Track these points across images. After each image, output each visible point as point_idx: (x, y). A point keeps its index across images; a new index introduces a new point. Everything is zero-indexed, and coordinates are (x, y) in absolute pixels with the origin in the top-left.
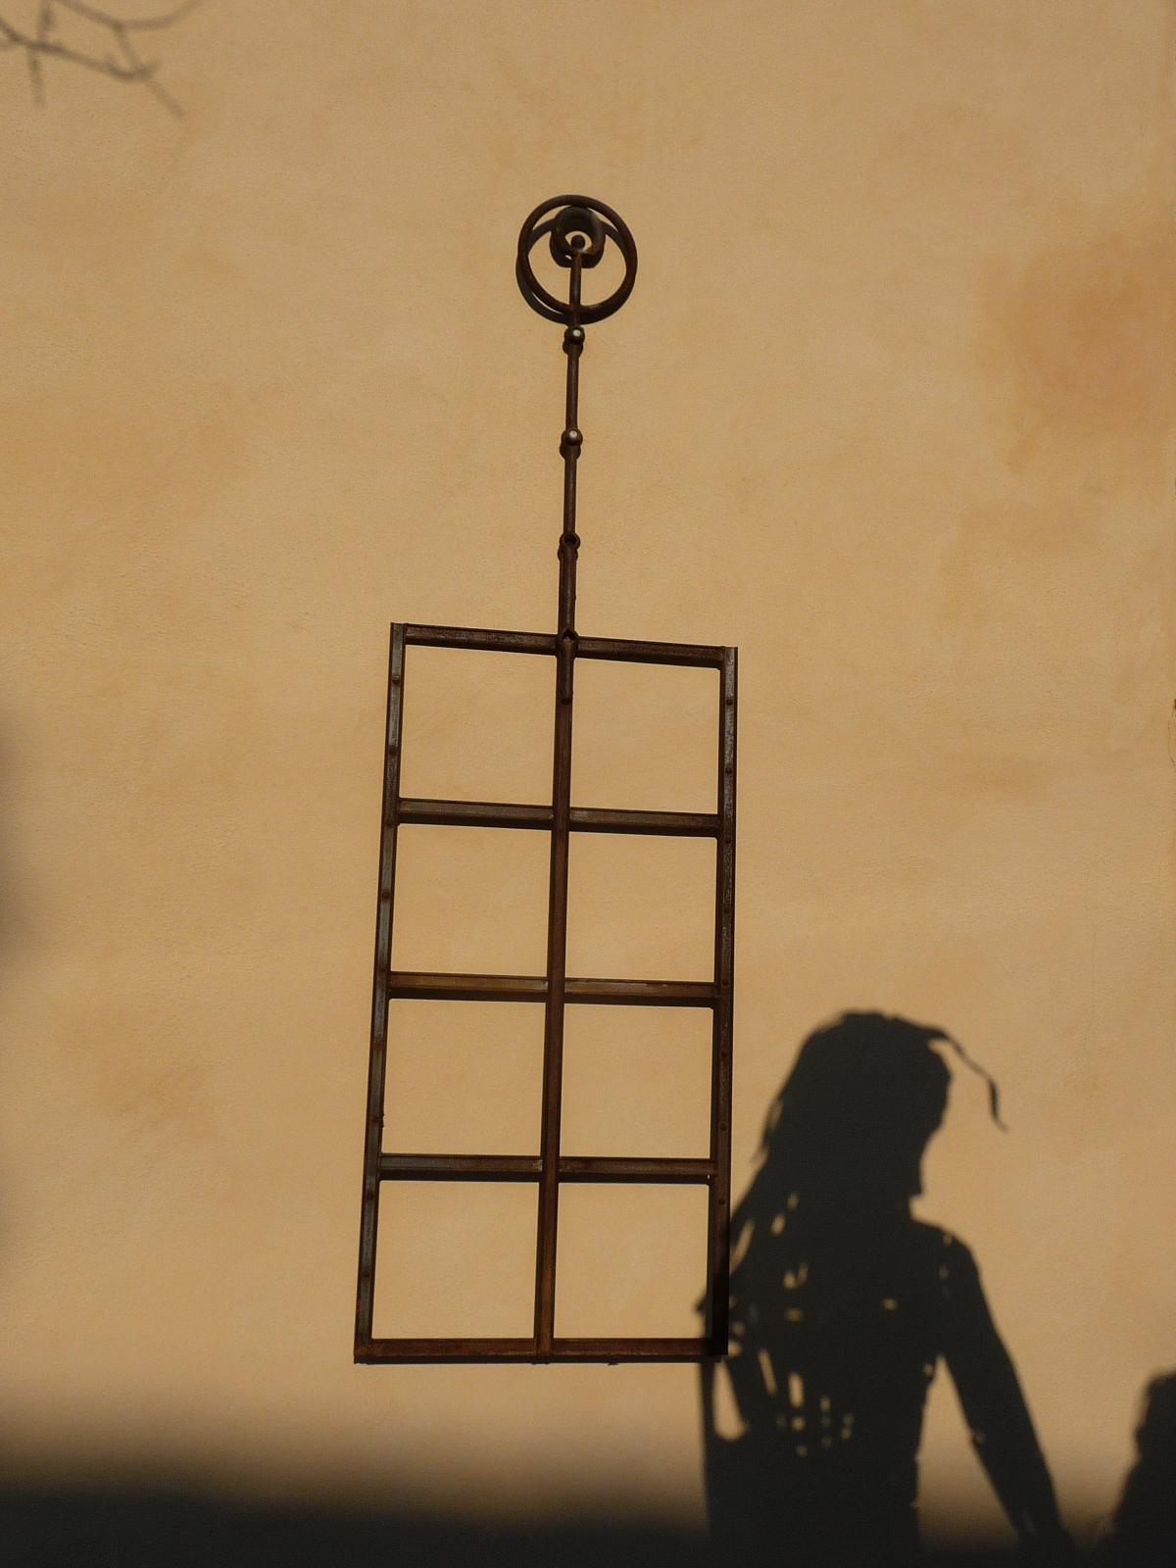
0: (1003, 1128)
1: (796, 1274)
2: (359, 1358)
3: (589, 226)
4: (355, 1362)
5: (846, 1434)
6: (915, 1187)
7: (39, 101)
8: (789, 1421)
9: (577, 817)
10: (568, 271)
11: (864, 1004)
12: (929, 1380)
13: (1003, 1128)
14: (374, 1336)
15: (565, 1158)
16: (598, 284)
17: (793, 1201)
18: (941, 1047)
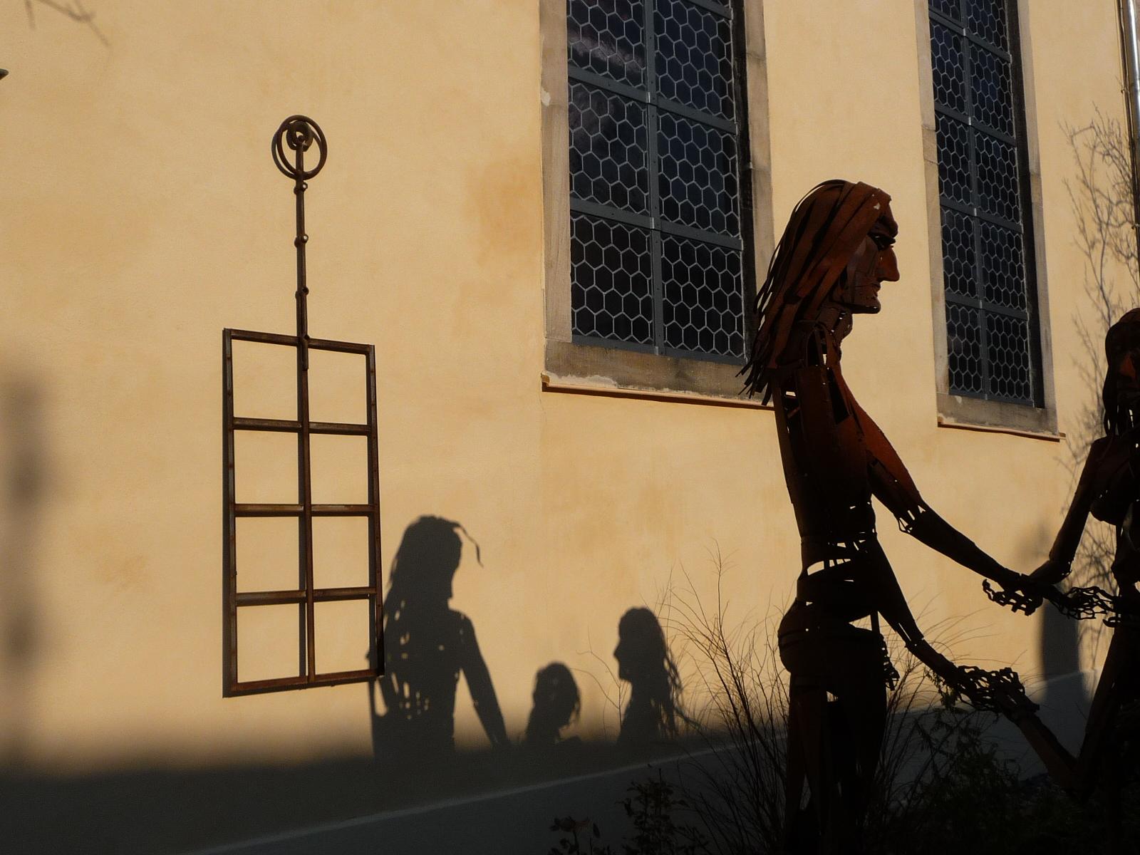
0: (482, 566)
1: (405, 638)
2: (543, 391)
3: (305, 131)
4: (224, 697)
5: (426, 708)
6: (449, 594)
7: (32, 26)
8: (404, 704)
9: (312, 426)
10: (295, 152)
11: (428, 512)
12: (456, 680)
13: (482, 566)
14: (239, 682)
15: (316, 590)
16: (311, 158)
17: (403, 604)
18: (458, 531)
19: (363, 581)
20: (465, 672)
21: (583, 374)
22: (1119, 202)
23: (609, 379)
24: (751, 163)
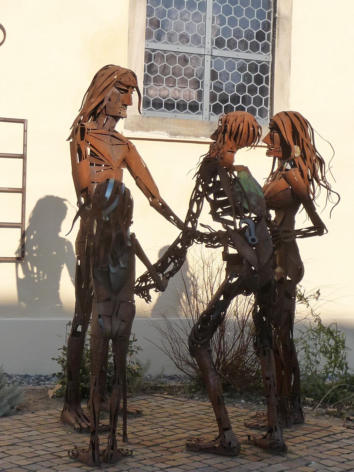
11: (50, 194)
17: (35, 232)
18: (65, 202)
19: (18, 220)
20: (67, 265)
21: (148, 130)
22: (170, 131)
23: (164, 133)
24: (277, 14)
